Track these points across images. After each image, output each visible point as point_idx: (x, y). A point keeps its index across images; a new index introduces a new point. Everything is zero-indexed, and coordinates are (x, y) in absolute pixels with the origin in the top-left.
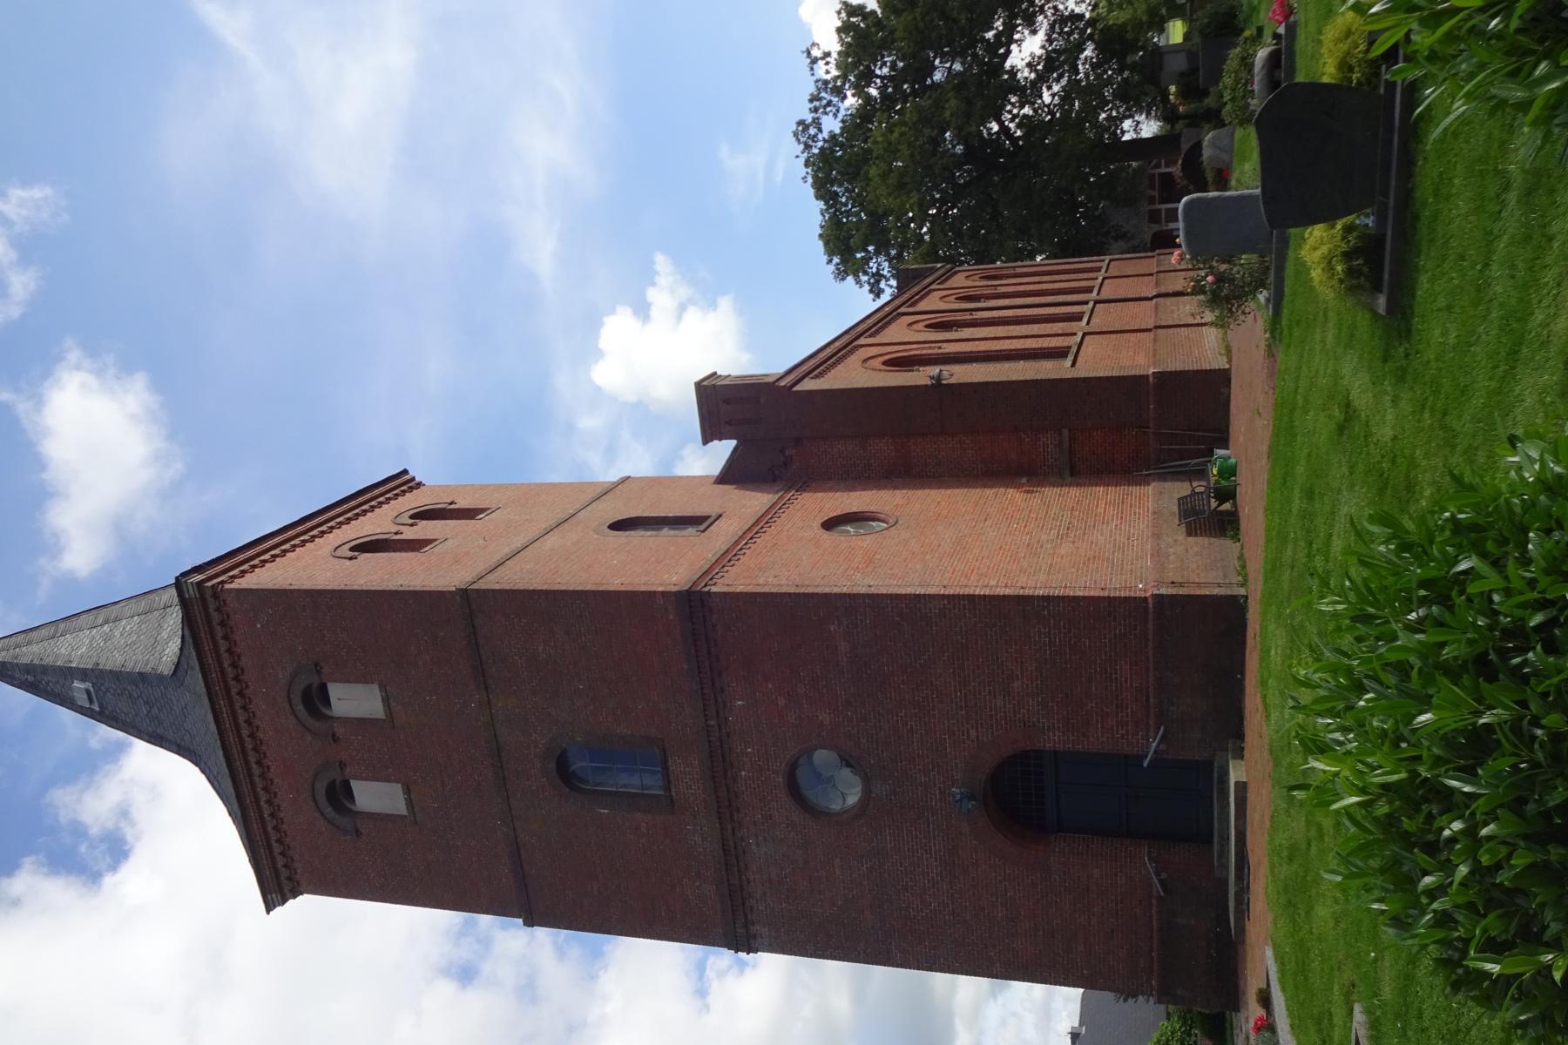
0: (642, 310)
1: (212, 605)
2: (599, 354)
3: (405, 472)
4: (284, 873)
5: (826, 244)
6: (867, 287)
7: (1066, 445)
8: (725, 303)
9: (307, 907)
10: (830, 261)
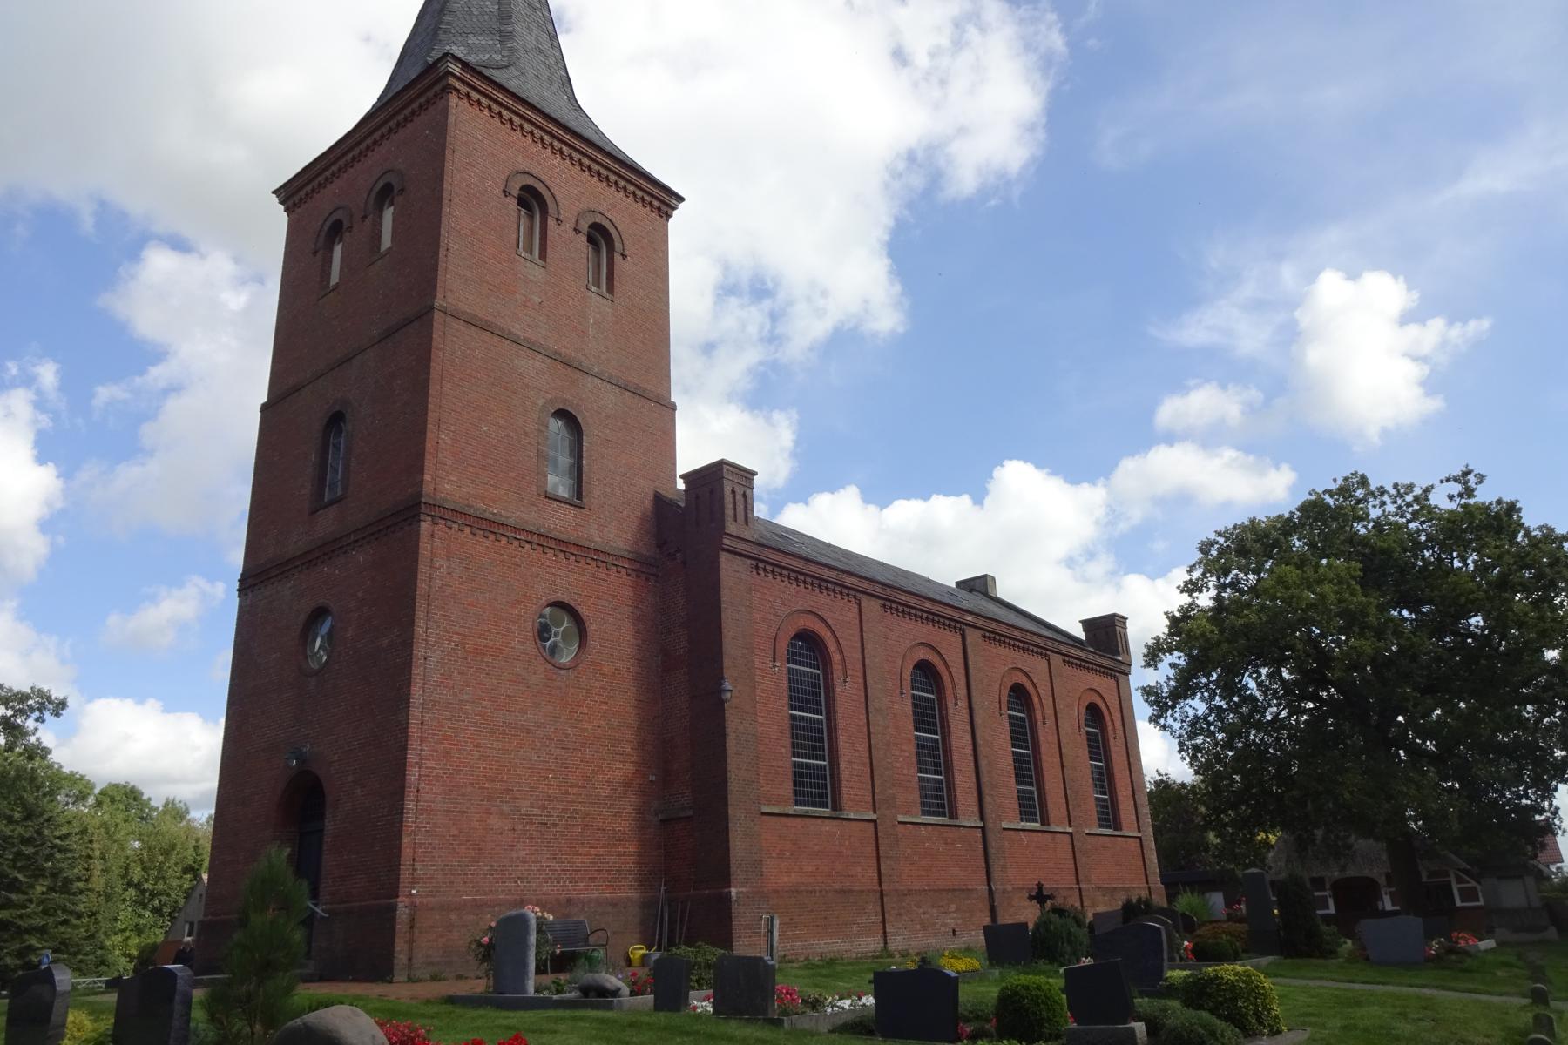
0: (1408, 318)
1: (437, 88)
2: (1353, 275)
3: (663, 200)
4: (296, 199)
5: (1243, 527)
6: (1188, 578)
7: (682, 814)
8: (1434, 404)
9: (278, 219)
10: (1219, 534)
